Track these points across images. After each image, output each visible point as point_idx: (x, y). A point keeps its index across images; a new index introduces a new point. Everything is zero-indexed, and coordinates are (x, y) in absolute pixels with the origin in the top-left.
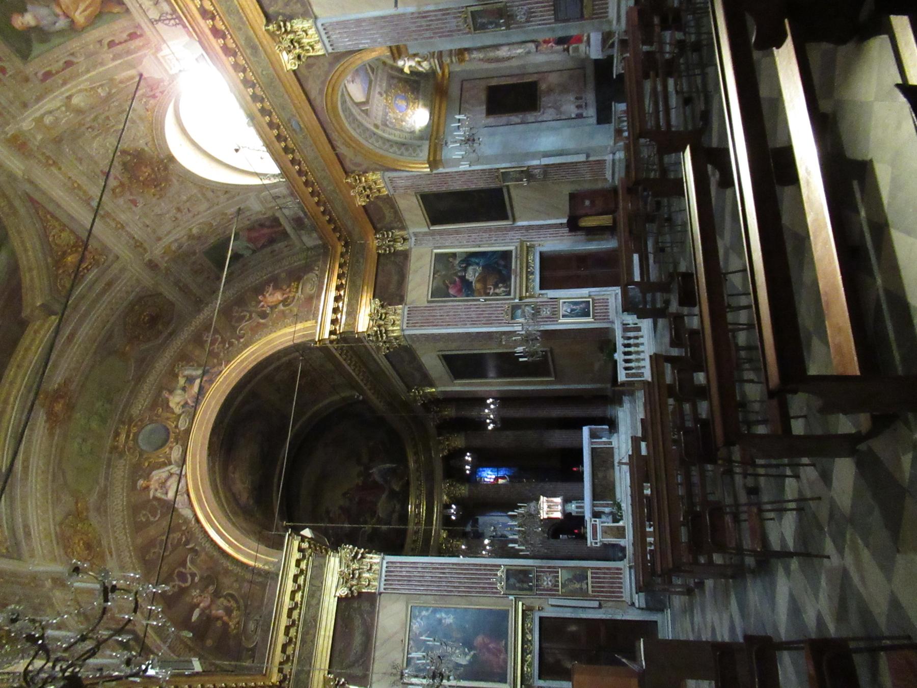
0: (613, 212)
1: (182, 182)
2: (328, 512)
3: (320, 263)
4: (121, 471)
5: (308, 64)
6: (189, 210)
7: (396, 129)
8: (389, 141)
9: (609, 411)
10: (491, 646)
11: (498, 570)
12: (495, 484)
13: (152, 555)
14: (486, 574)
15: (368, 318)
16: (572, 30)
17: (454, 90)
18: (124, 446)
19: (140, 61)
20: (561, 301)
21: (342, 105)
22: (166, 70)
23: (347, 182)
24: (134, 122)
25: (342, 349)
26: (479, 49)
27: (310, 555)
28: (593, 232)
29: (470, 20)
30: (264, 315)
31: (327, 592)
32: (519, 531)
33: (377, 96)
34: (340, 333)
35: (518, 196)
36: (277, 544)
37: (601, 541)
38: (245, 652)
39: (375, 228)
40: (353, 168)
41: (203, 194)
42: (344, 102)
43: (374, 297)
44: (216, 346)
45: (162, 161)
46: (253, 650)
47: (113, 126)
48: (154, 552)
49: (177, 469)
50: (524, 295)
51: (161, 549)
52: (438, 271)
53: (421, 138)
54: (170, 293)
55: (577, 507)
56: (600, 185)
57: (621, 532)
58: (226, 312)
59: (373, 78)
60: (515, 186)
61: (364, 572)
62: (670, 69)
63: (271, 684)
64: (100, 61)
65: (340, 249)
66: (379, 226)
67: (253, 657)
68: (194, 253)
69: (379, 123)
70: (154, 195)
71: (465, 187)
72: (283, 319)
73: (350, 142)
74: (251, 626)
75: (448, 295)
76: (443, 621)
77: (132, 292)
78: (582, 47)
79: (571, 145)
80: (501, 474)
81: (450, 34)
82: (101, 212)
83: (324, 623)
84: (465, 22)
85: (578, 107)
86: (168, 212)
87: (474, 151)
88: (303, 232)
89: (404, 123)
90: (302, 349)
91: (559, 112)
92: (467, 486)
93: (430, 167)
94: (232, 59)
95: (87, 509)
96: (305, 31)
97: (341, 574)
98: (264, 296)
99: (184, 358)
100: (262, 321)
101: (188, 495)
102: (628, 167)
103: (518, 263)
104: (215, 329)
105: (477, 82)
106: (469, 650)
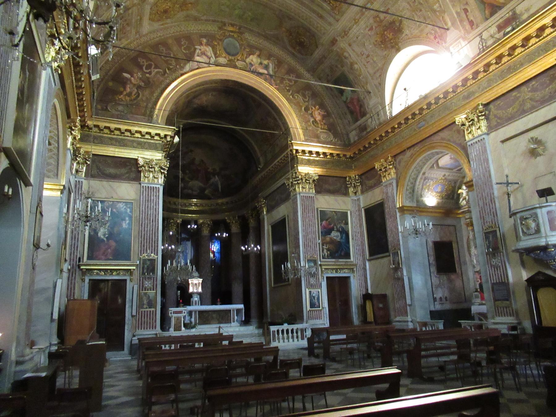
0: (376, 322)
1: (385, 58)
2: (191, 151)
3: (339, 142)
4: (212, 28)
5: (460, 131)
6: (368, 62)
7: (423, 186)
8: (415, 181)
9: (254, 321)
10: (109, 250)
11: (155, 254)
12: (208, 250)
13: (162, 48)
14: (152, 246)
15: (307, 172)
16: (487, 294)
17: (449, 221)
18: (226, 30)
19: (457, 28)
20: (320, 290)
21: (436, 152)
22: (451, 45)
23: (389, 157)
24: (419, 26)
25: (287, 157)
26: (474, 235)
27: (163, 142)
28: (363, 309)
29: (491, 230)
30: (307, 109)
31: (141, 152)
32: (178, 267)
33: (443, 173)
34: (297, 156)
35: (384, 262)
36: (169, 121)
37: (172, 316)
38: (105, 105)
39: (362, 175)
40: (398, 160)
41: (378, 70)
42: (437, 153)
43: (319, 176)
44: (287, 82)
45: (398, 45)
46: (106, 109)
47: (417, 15)
48: (163, 50)
49: (213, 61)
50: (323, 267)
51: (166, 54)
52: (336, 214)
53: (418, 201)
54: (317, 53)
55: (196, 301)
56: (392, 313)
57: (178, 328)
58: (308, 87)
59: (454, 170)
60: (390, 261)
61: (153, 174)
62: (463, 357)
63: (86, 120)
64: (455, 5)
65: (348, 154)
66: (363, 177)
67: (102, 109)
68: (342, 66)
69: (426, 175)
70: (376, 41)
71: (388, 229)
72: (304, 121)
73: (413, 158)
74: (120, 108)
75: (322, 221)
76: (124, 222)
77: (318, 31)
78: (479, 300)
79: (416, 294)
80: (216, 255)
81: (482, 218)
82: (364, 10)
83: (123, 151)
84: (489, 227)
85: (441, 298)
86: (366, 50)
87: (410, 235)
88: (358, 131)
89: (427, 190)
90: (286, 133)
91: (437, 287)
92: (209, 234)
93: (400, 208)
94: (460, 84)
95: (188, 10)
96: (479, 128)
97: (152, 160)
98: (318, 109)
99: (279, 63)
100: (303, 108)
101: (197, 69)
102: (403, 331)
103: (343, 263)
104: (297, 81)
105: (455, 236)
106: (107, 238)
